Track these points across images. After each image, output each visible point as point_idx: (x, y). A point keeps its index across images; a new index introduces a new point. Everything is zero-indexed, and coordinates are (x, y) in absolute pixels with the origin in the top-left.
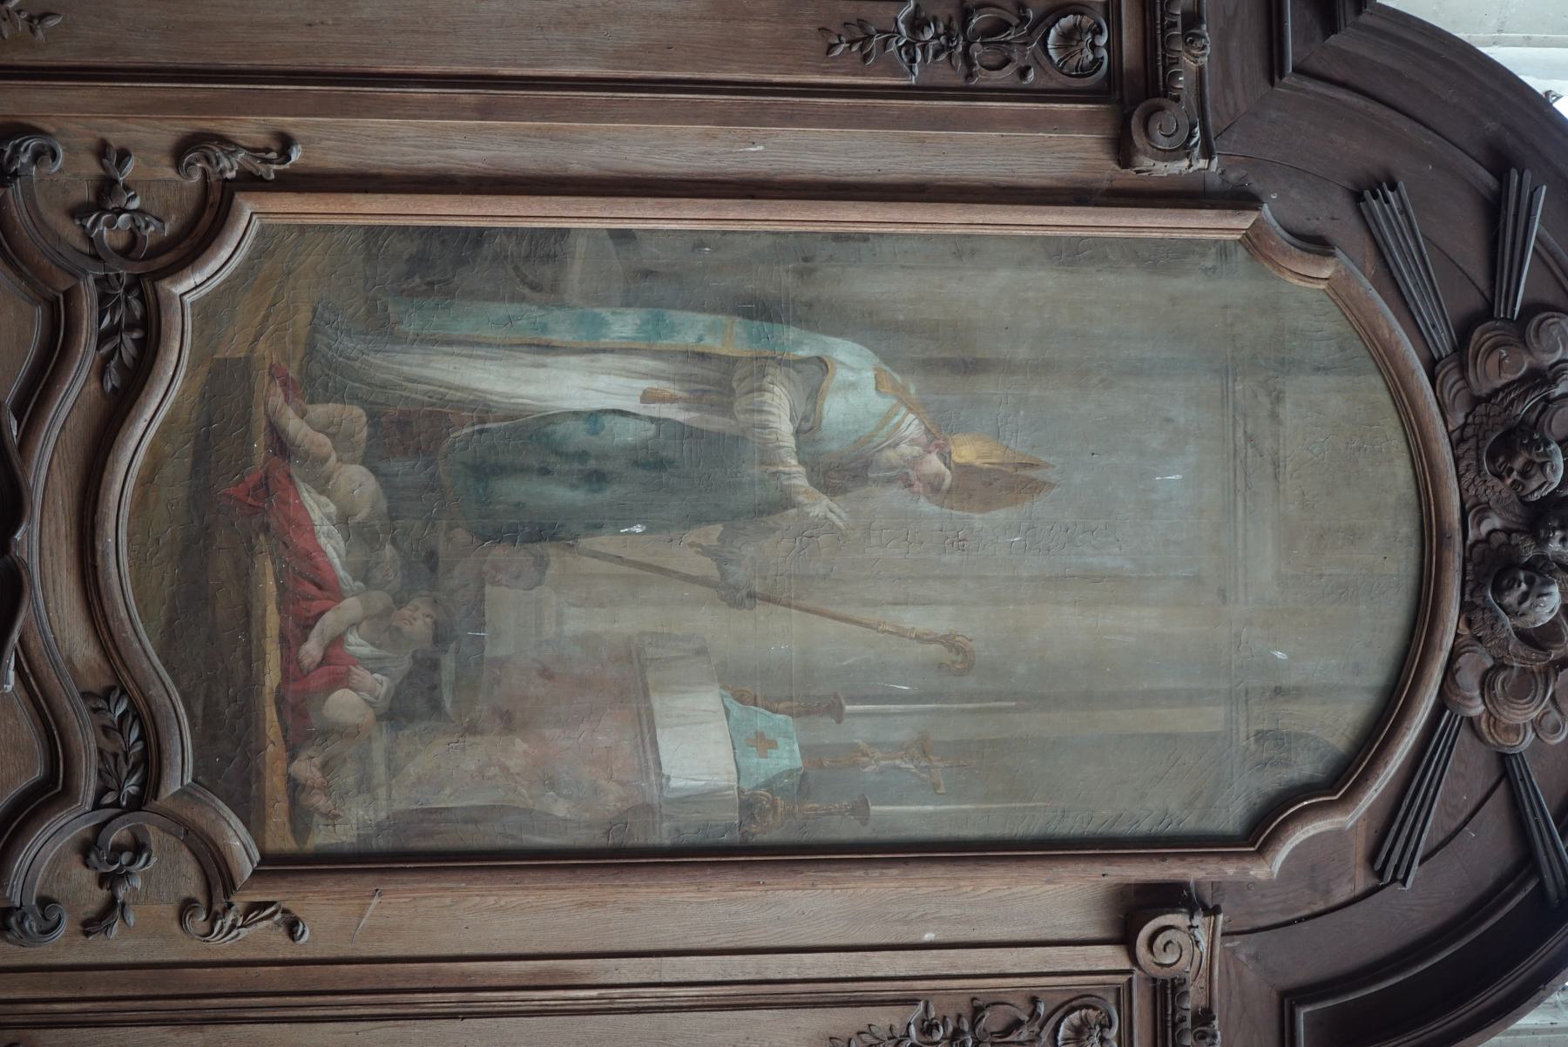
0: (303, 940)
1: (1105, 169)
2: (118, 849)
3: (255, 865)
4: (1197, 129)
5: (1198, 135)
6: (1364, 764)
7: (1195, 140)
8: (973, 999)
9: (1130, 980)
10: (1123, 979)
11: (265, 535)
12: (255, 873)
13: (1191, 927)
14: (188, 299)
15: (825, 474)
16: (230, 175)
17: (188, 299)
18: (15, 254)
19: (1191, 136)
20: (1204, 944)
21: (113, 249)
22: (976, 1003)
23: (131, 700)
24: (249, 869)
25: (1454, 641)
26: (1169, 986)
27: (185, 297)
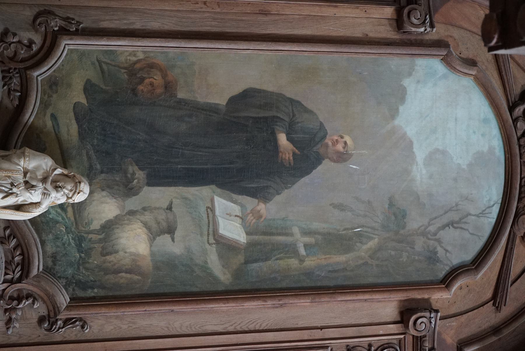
0: (86, 331)
1: (390, 34)
2: (12, 298)
3: (68, 303)
4: (428, 16)
5: (428, 19)
6: (487, 251)
7: (427, 21)
8: (347, 346)
9: (405, 337)
10: (402, 336)
11: (438, 263)
12: (67, 307)
13: (430, 317)
14: (40, 79)
15: (121, 169)
16: (56, 29)
17: (40, 79)
18: (202, 307)
19: (426, 20)
20: (434, 323)
21: (8, 57)
22: (348, 347)
23: (18, 240)
24: (65, 305)
25: (517, 205)
26: (419, 338)
27: (38, 78)
